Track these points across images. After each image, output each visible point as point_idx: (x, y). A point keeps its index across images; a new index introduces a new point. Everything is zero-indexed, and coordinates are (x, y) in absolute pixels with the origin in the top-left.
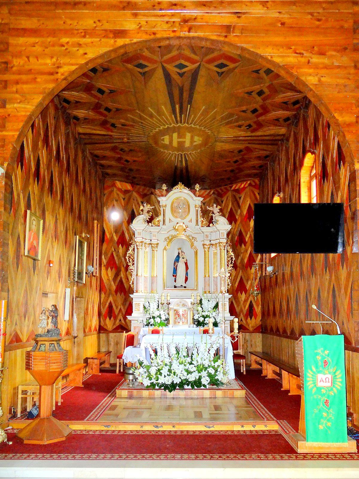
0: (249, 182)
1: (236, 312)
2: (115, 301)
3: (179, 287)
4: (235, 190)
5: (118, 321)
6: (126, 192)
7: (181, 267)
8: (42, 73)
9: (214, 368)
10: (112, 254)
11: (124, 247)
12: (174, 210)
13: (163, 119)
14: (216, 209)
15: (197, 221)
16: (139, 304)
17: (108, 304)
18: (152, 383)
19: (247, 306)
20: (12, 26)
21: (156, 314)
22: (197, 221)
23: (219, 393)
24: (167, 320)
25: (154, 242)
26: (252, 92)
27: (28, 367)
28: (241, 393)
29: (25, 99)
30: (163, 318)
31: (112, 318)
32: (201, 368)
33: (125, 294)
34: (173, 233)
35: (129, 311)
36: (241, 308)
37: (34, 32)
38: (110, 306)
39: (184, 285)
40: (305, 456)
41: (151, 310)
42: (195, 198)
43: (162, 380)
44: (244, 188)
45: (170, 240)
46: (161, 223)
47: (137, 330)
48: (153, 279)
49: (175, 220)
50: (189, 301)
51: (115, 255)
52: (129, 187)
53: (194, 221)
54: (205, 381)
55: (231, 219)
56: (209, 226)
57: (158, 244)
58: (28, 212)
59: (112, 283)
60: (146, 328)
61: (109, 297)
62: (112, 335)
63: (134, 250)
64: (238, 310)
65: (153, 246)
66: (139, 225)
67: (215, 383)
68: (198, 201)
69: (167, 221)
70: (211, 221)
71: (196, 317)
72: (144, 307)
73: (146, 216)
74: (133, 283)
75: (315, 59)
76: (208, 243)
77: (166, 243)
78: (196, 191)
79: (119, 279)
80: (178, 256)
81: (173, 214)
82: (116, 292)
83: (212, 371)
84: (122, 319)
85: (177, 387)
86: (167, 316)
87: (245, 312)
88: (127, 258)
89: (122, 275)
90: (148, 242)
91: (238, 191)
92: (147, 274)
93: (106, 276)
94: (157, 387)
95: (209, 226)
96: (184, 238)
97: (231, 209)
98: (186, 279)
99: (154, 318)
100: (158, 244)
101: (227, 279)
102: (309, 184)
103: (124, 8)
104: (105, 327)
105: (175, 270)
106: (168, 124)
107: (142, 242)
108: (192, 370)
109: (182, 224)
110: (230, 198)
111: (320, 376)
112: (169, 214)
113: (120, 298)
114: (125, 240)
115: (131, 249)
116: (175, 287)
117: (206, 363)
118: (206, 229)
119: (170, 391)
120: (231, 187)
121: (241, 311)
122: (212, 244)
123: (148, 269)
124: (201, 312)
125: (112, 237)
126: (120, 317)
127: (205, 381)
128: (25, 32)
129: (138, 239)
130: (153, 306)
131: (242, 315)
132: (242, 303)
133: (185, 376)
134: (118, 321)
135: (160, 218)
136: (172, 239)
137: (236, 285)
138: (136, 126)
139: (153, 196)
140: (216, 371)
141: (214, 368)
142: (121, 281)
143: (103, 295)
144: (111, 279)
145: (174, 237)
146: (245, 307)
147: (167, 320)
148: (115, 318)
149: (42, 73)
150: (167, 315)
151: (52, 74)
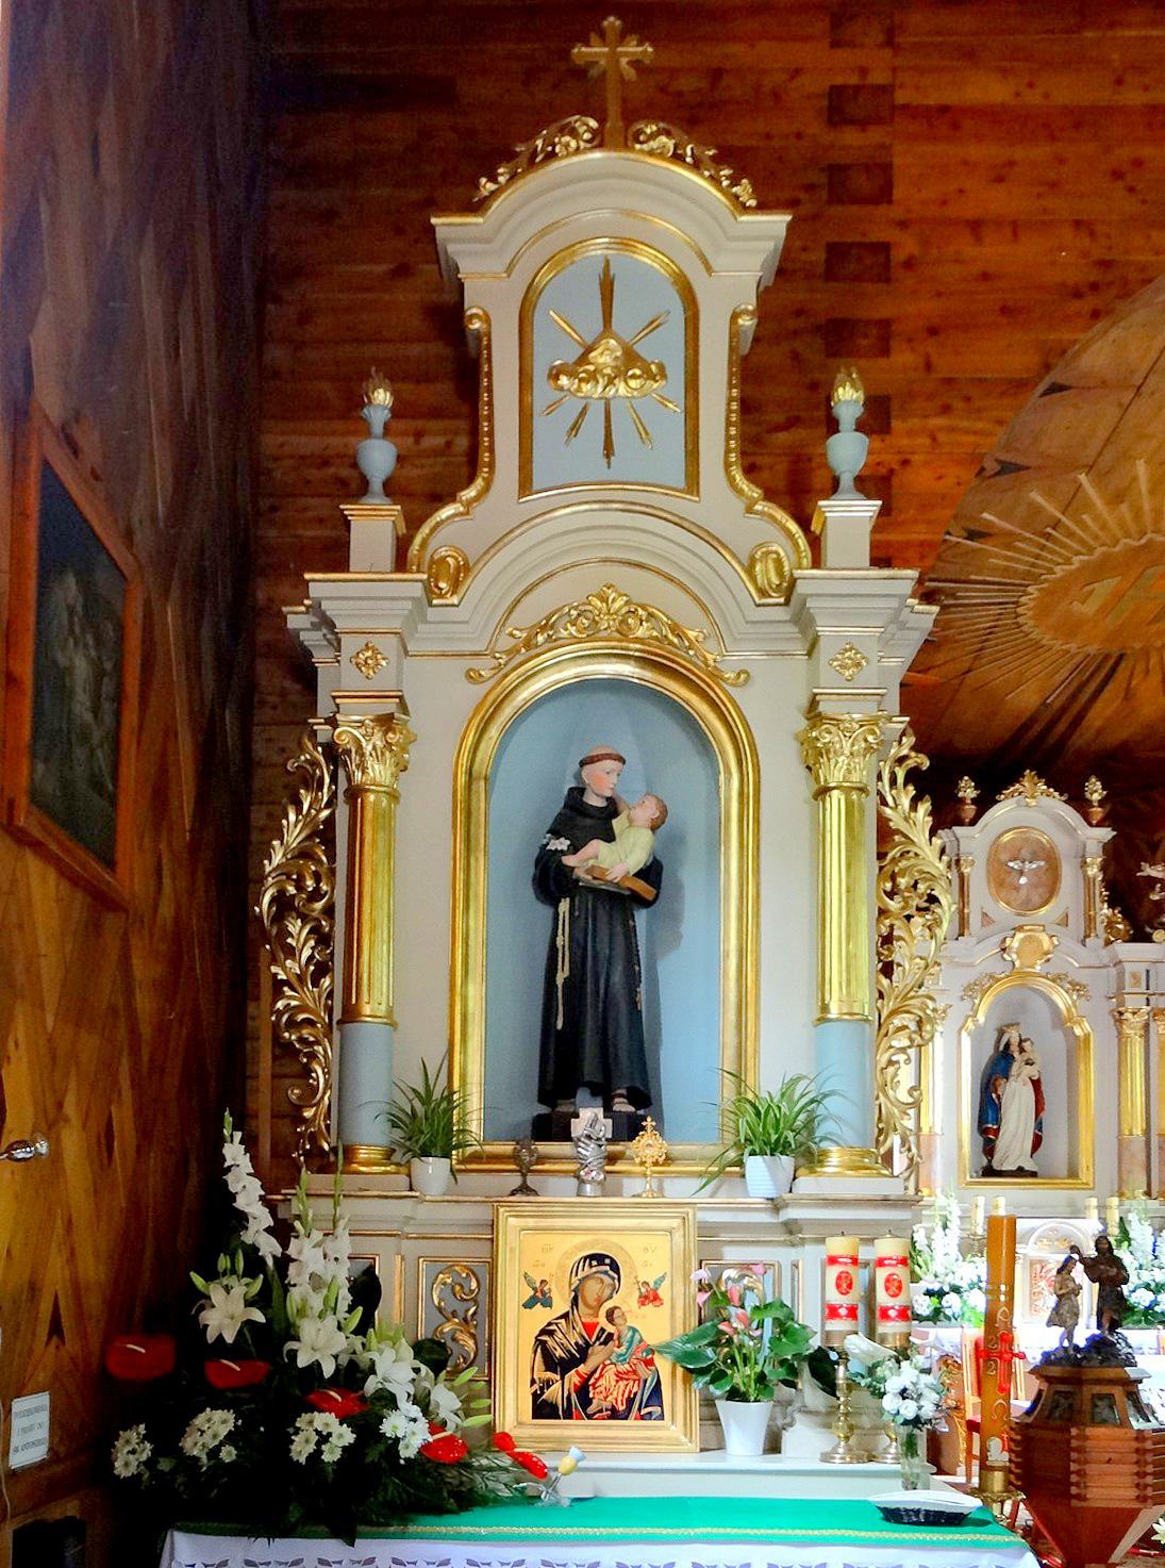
7: (1016, 1098)
12: (1001, 879)
13: (1085, 527)
15: (1090, 921)
26: (998, 473)
39: (1029, 1166)
53: (1077, 923)
69: (975, 920)
78: (1089, 803)
98: (1037, 1142)
99: (956, 1290)
102: (152, 882)
106: (1078, 553)
128: (946, 119)
138: (1025, 540)
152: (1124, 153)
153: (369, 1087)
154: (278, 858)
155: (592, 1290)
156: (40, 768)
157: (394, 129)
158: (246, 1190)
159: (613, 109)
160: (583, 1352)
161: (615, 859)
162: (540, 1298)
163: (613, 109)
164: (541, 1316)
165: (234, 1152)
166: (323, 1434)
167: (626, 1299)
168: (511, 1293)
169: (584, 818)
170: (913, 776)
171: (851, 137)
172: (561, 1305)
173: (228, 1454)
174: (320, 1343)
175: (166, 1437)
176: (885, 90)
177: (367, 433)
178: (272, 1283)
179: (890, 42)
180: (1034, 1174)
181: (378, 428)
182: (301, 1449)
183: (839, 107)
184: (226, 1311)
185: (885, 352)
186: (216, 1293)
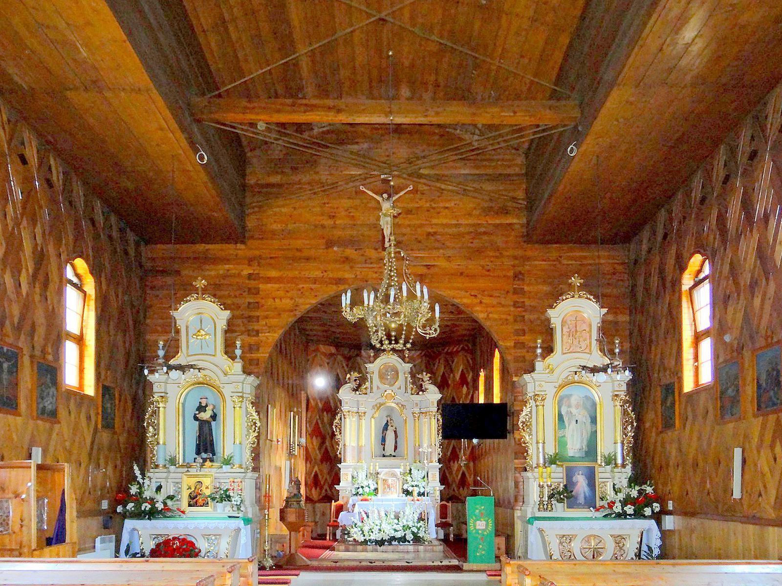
0: (461, 346)
1: (448, 482)
2: (321, 471)
3: (387, 456)
4: (447, 353)
5: (324, 491)
6: (332, 355)
7: (390, 436)
8: (285, 311)
9: (417, 527)
10: (317, 422)
11: (329, 415)
12: (382, 377)
14: (426, 377)
15: (406, 389)
16: (347, 475)
17: (313, 474)
18: (365, 540)
19: (460, 476)
20: (261, 276)
21: (365, 483)
22: (406, 389)
23: (421, 548)
24: (376, 490)
25: (362, 410)
27: (282, 519)
28: (441, 548)
29: (271, 329)
30: (373, 487)
31: (318, 489)
32: (406, 528)
33: (331, 463)
34: (381, 400)
35: (337, 481)
36: (454, 478)
37: (278, 280)
38: (316, 475)
39: (393, 454)
40: (466, 571)
41: (360, 479)
42: (404, 364)
43: (373, 537)
44: (457, 352)
45: (378, 406)
46: (369, 390)
47: (345, 499)
48: (360, 449)
49: (384, 387)
50: (398, 471)
51: (319, 422)
52: (333, 350)
54: (410, 537)
55: (442, 385)
56: (418, 394)
57: (365, 413)
58: (269, 406)
59: (318, 452)
60: (355, 498)
61: (314, 467)
62: (318, 505)
63: (341, 419)
64: (450, 479)
65: (360, 415)
66: (345, 394)
67: (417, 540)
68: (408, 366)
69: (375, 388)
70: (420, 389)
71: (405, 487)
72: (353, 477)
73: (353, 385)
74: (340, 453)
75: (486, 300)
76: (417, 410)
77: (374, 411)
79: (324, 447)
80: (387, 425)
81: (381, 382)
82: (322, 461)
83: (415, 530)
84: (328, 489)
85: (386, 543)
86: (376, 486)
87: (457, 481)
88: (334, 427)
89: (327, 443)
90: (355, 410)
91: (451, 354)
92: (354, 444)
93: (311, 445)
94: (369, 543)
95: (418, 394)
96: (393, 405)
97: (444, 373)
99: (362, 487)
100: (365, 413)
101: (437, 448)
103: (344, 262)
104: (311, 497)
105: (384, 440)
107: (349, 412)
108: (398, 529)
109: (390, 392)
110: (442, 361)
111: (478, 522)
112: (376, 381)
113: (325, 467)
114: (330, 408)
115: (338, 417)
116: (384, 456)
117: (411, 524)
118: (416, 398)
119: (380, 546)
120: (443, 350)
121: (454, 481)
122: (423, 413)
123: (356, 435)
124: (410, 482)
125: (317, 404)
126: (326, 487)
127: (410, 537)
128: (269, 280)
129: (345, 408)
130: (362, 476)
131: (454, 485)
132: (454, 472)
133: (393, 534)
134: (324, 491)
135: (368, 384)
136: (380, 406)
137: (449, 453)
139: (358, 358)
140: (419, 529)
141: (417, 527)
142: (326, 449)
143: (308, 465)
144: (317, 448)
145: (381, 405)
146: (457, 476)
147: (376, 490)
148: (321, 488)
149: (285, 311)
150: (376, 485)
151: (292, 311)
152: (301, 286)
153: (160, 454)
154: (147, 416)
155: (198, 487)
156: (109, 372)
157: (169, 280)
158: (137, 472)
159: (200, 293)
160: (196, 496)
161: (205, 416)
162: (190, 488)
163: (200, 293)
164: (190, 491)
165: (136, 467)
166: (146, 506)
167: (203, 488)
168: (185, 487)
169: (201, 408)
170: (252, 403)
171: (252, 282)
172: (193, 489)
173: (133, 509)
174: (147, 494)
175: (125, 506)
176: (258, 274)
177: (159, 349)
178: (141, 486)
179: (259, 265)
180: (394, 456)
181: (161, 348)
182: (143, 509)
183: (250, 276)
184: (134, 490)
185: (258, 322)
186: (132, 487)
